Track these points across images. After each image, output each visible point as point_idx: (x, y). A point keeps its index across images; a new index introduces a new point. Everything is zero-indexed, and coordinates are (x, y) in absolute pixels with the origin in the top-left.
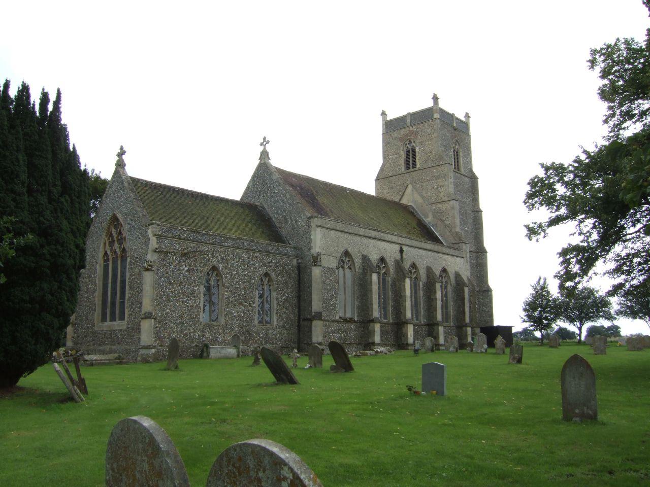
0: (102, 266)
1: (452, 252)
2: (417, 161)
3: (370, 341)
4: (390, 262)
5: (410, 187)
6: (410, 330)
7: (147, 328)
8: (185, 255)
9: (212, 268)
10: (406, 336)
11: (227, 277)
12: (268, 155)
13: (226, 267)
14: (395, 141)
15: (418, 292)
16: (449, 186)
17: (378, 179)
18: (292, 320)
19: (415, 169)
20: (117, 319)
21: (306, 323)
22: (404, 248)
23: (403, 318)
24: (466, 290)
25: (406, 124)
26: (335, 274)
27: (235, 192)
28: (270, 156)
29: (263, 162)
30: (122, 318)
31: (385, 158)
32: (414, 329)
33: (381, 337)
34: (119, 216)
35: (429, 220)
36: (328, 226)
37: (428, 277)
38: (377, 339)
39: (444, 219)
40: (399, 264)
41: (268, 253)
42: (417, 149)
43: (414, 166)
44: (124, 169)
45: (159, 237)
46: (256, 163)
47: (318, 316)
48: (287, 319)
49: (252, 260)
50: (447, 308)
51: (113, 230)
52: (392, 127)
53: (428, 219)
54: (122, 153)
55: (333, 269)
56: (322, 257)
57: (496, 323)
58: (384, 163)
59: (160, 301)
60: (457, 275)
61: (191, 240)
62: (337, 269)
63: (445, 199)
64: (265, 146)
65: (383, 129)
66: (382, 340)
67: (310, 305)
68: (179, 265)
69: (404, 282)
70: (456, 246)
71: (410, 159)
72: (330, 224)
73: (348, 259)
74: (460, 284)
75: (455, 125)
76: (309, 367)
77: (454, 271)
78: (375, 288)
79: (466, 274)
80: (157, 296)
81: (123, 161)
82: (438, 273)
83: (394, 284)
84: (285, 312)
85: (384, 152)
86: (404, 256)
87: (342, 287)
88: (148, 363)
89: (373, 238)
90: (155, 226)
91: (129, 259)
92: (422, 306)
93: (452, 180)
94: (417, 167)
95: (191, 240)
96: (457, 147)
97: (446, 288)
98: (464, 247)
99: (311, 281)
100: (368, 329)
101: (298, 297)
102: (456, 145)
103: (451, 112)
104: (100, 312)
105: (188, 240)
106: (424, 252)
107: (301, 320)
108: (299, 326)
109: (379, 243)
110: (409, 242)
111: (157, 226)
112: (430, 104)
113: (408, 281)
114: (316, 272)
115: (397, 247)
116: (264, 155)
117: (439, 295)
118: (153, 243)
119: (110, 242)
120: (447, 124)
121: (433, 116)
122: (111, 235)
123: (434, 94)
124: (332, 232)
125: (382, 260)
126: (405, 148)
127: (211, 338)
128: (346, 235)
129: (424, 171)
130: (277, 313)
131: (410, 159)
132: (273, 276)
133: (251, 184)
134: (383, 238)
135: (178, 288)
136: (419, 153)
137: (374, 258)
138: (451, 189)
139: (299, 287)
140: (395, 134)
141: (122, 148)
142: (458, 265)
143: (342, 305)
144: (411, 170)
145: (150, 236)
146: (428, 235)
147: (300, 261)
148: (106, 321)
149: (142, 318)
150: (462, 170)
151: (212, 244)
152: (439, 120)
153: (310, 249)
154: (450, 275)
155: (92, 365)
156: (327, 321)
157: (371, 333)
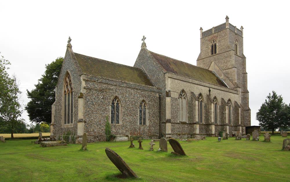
1: (233, 91)
2: (217, 50)
3: (194, 133)
4: (204, 96)
5: (213, 63)
6: (213, 128)
7: (80, 126)
8: (102, 91)
9: (115, 97)
10: (211, 130)
11: (123, 102)
12: (145, 45)
13: (122, 97)
15: (217, 110)
16: (233, 60)
17: (198, 60)
19: (216, 54)
21: (163, 124)
22: (211, 89)
23: (210, 122)
24: (240, 109)
25: (212, 33)
26: (177, 101)
27: (131, 62)
28: (146, 45)
30: (72, 122)
31: (201, 50)
32: (215, 127)
33: (199, 131)
34: (69, 72)
35: (222, 78)
36: (174, 77)
37: (222, 103)
38: (197, 131)
39: (229, 76)
40: (209, 96)
41: (144, 90)
42: (217, 44)
43: (215, 53)
44: (71, 48)
45: (86, 81)
46: (139, 49)
47: (169, 121)
48: (154, 122)
49: (136, 94)
50: (230, 117)
51: (67, 79)
52: (205, 35)
53: (221, 77)
54: (70, 40)
55: (176, 99)
56: (171, 92)
57: (252, 125)
58: (201, 52)
59: (86, 114)
60: (236, 102)
61: (104, 83)
62: (179, 98)
63: (230, 67)
65: (201, 36)
66: (200, 132)
67: (165, 116)
68: (98, 95)
69: (211, 105)
70: (235, 89)
71: (214, 49)
72: (175, 76)
73: (184, 94)
74: (237, 106)
75: (236, 32)
76: (160, 151)
77: (234, 101)
78: (197, 108)
79: (239, 102)
80: (86, 110)
81: (70, 44)
82: (226, 101)
83: (205, 106)
84: (153, 119)
85: (201, 47)
86: (211, 93)
87: (181, 108)
89: (196, 84)
90: (84, 75)
91: (73, 93)
92: (219, 117)
93: (234, 58)
94: (217, 53)
95: (104, 83)
96: (236, 43)
97: (230, 108)
98: (239, 90)
99: (165, 104)
100: (193, 127)
101: (159, 112)
102: (236, 42)
105: (102, 83)
106: (220, 91)
107: (161, 123)
108: (160, 126)
109: (199, 86)
110: (213, 86)
111: (85, 76)
112: (224, 21)
113: (213, 104)
114: (168, 99)
115: (208, 89)
116: (144, 45)
117: (227, 112)
118: (84, 84)
119: (67, 85)
120: (233, 31)
121: (225, 27)
122: (67, 82)
123: (227, 16)
124: (176, 81)
125: (200, 95)
126: (211, 44)
127: (115, 131)
128: (183, 82)
130: (149, 120)
131: (214, 49)
132: (147, 102)
134: (201, 84)
135: (97, 107)
137: (197, 94)
138: (234, 63)
139: (160, 107)
140: (207, 38)
141: (70, 38)
142: (236, 98)
143: (181, 116)
144: (214, 54)
145: (82, 80)
146: (222, 84)
147: (160, 94)
148: (66, 124)
149: (78, 122)
150: (238, 54)
151: (115, 85)
152: (228, 29)
153: (165, 89)
154: (232, 102)
155: (46, 146)
156: (173, 123)
157: (194, 129)
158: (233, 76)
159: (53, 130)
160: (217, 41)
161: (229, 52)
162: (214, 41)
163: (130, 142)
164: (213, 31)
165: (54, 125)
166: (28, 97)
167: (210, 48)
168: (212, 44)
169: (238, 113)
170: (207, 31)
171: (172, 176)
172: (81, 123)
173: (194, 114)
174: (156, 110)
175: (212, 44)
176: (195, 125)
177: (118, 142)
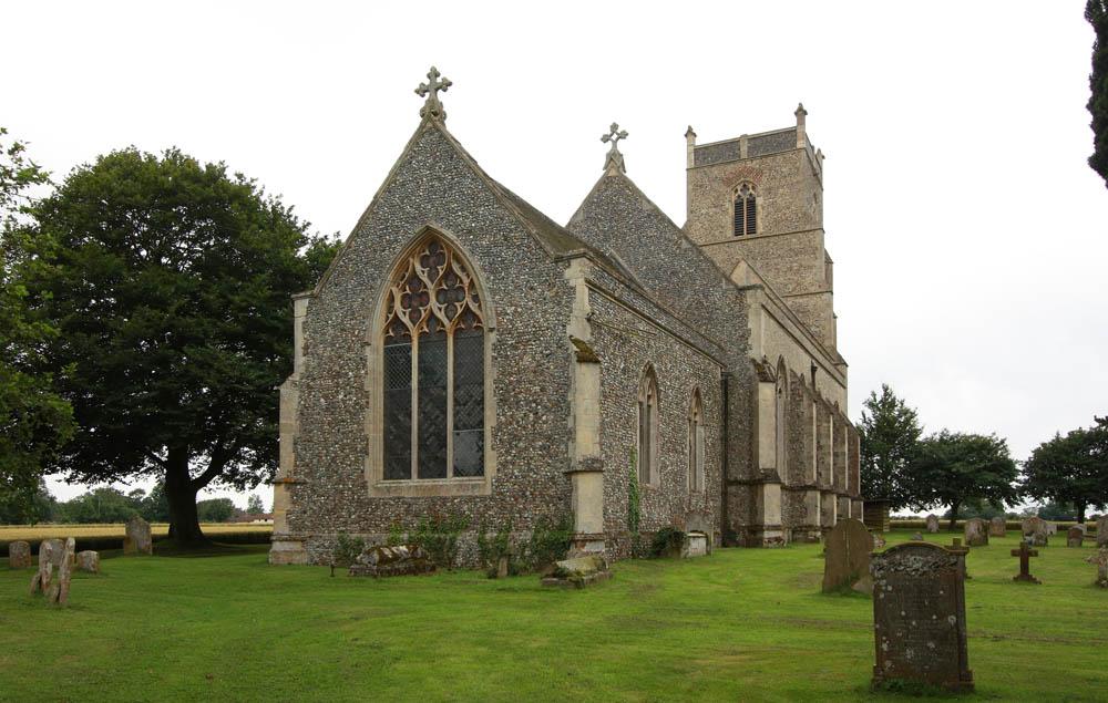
0: (382, 351)
5: (743, 265)
14: (715, 185)
18: (716, 482)
19: (753, 235)
20: (450, 473)
29: (613, 173)
42: (759, 201)
43: (752, 229)
46: (594, 173)
63: (812, 289)
64: (615, 143)
88: (12, 568)
91: (492, 338)
100: (801, 501)
103: (1092, 135)
104: (381, 456)
108: (725, 494)
112: (791, 122)
121: (795, 144)
126: (734, 198)
129: (772, 239)
133: (581, 217)
136: (763, 208)
140: (715, 171)
144: (745, 236)
158: (823, 323)
159: (289, 507)
160: (759, 188)
161: (810, 235)
163: (1017, 561)
164: (744, 149)
165: (295, 483)
167: (731, 211)
168: (739, 196)
169: (445, 461)
170: (717, 146)
172: (596, 475)
173: (805, 454)
174: (717, 434)
175: (739, 196)
176: (809, 493)
177: (692, 559)
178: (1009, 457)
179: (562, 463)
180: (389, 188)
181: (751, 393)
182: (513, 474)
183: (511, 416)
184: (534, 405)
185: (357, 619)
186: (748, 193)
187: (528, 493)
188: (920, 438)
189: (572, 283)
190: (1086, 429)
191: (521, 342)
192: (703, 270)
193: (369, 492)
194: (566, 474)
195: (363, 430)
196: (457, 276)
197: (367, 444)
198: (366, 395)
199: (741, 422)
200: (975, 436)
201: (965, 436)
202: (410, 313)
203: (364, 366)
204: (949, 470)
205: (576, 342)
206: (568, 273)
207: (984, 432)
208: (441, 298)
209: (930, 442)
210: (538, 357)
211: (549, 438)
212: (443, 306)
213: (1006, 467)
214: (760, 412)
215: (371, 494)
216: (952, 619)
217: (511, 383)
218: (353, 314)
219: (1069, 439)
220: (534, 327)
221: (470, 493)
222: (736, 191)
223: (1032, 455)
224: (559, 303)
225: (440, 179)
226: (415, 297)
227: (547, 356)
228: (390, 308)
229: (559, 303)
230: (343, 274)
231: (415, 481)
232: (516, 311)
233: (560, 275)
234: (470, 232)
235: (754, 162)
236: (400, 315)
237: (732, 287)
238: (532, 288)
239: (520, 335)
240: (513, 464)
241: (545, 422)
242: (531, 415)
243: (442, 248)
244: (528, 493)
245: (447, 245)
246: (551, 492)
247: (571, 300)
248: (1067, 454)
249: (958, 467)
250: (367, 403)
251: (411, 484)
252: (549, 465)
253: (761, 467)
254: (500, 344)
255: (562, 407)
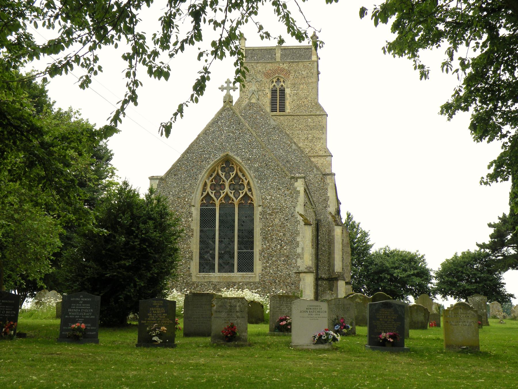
14: (259, 76)
42: (288, 91)
43: (283, 109)
121: (310, 57)
126: (271, 86)
129: (296, 118)
161: (320, 118)
162: (278, 79)
166: (488, 142)
167: (269, 95)
171: (109, 377)
178: (427, 267)
179: (293, 268)
180: (206, 132)
181: (330, 231)
182: (270, 272)
183: (269, 246)
184: (280, 241)
185: (31, 366)
186: (280, 84)
187: (277, 281)
188: (372, 251)
189: (298, 189)
190: (473, 251)
191: (274, 212)
192: (303, 162)
193: (193, 278)
194: (296, 273)
195: (190, 248)
196: (240, 178)
197: (192, 255)
198: (192, 231)
199: (324, 246)
200: (396, 251)
201: (399, 251)
202: (215, 193)
203: (191, 216)
204: (392, 275)
205: (301, 215)
206: (296, 184)
207: (412, 250)
208: (232, 187)
209: (377, 255)
210: (282, 220)
211: (287, 256)
212: (233, 191)
213: (424, 274)
214: (335, 241)
215: (194, 279)
216: (485, 311)
217: (269, 230)
218: (185, 190)
219: (463, 258)
220: (280, 206)
221: (248, 280)
222: (273, 82)
223: (440, 267)
224: (292, 197)
225: (233, 132)
226: (217, 185)
227: (287, 220)
228: (204, 190)
229: (292, 197)
230: (179, 170)
231: (217, 274)
232: (271, 198)
233: (292, 184)
234: (249, 160)
235: (285, 65)
236: (210, 194)
237: (319, 173)
238: (279, 189)
239: (273, 209)
240: (270, 267)
241: (285, 249)
242: (279, 246)
243: (232, 164)
244: (277, 281)
245: (236, 163)
246: (288, 281)
247: (296, 198)
248: (463, 267)
249: (397, 273)
250: (193, 235)
251: (216, 275)
252: (287, 268)
253: (336, 271)
254: (263, 213)
255: (293, 243)
